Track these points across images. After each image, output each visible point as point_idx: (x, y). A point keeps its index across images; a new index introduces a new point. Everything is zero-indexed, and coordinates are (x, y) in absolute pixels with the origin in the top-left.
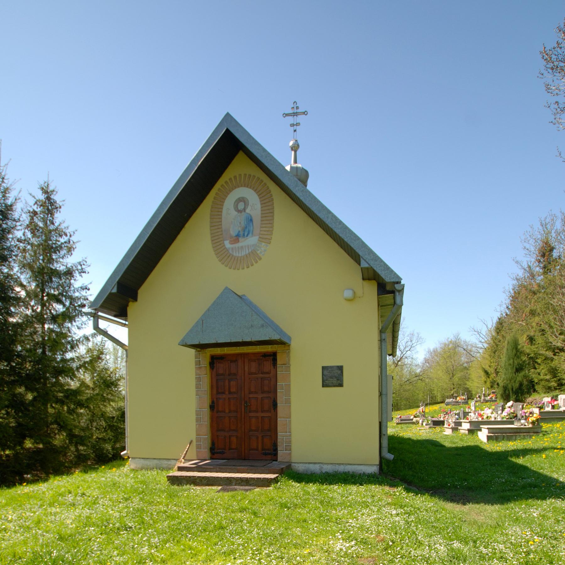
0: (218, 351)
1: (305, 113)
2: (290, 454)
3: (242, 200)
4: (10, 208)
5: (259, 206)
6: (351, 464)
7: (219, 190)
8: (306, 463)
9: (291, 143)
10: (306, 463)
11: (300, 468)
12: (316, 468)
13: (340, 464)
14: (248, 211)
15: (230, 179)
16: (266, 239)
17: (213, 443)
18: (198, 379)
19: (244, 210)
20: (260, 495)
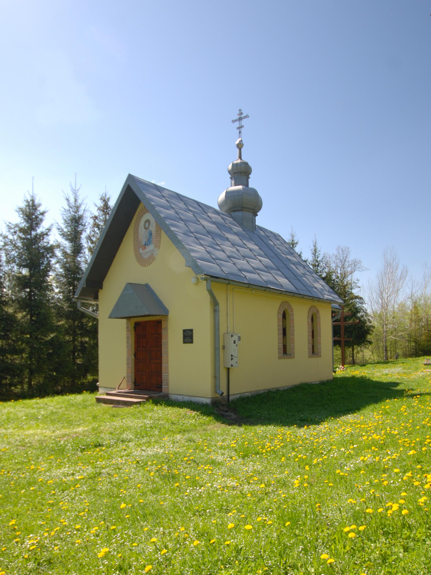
0: (139, 319)
1: (247, 117)
2: (168, 388)
3: (148, 221)
4: (81, 217)
5: (154, 225)
6: (197, 397)
7: (137, 218)
8: (178, 395)
9: (237, 142)
10: (178, 395)
11: (173, 397)
12: (180, 398)
13: (192, 396)
14: (150, 228)
15: (142, 208)
16: (158, 246)
17: (135, 380)
18: (128, 338)
19: (148, 227)
20: (329, 433)
